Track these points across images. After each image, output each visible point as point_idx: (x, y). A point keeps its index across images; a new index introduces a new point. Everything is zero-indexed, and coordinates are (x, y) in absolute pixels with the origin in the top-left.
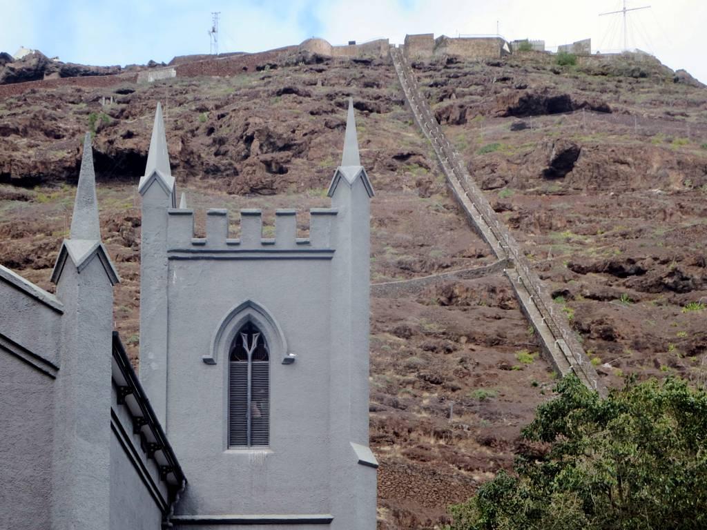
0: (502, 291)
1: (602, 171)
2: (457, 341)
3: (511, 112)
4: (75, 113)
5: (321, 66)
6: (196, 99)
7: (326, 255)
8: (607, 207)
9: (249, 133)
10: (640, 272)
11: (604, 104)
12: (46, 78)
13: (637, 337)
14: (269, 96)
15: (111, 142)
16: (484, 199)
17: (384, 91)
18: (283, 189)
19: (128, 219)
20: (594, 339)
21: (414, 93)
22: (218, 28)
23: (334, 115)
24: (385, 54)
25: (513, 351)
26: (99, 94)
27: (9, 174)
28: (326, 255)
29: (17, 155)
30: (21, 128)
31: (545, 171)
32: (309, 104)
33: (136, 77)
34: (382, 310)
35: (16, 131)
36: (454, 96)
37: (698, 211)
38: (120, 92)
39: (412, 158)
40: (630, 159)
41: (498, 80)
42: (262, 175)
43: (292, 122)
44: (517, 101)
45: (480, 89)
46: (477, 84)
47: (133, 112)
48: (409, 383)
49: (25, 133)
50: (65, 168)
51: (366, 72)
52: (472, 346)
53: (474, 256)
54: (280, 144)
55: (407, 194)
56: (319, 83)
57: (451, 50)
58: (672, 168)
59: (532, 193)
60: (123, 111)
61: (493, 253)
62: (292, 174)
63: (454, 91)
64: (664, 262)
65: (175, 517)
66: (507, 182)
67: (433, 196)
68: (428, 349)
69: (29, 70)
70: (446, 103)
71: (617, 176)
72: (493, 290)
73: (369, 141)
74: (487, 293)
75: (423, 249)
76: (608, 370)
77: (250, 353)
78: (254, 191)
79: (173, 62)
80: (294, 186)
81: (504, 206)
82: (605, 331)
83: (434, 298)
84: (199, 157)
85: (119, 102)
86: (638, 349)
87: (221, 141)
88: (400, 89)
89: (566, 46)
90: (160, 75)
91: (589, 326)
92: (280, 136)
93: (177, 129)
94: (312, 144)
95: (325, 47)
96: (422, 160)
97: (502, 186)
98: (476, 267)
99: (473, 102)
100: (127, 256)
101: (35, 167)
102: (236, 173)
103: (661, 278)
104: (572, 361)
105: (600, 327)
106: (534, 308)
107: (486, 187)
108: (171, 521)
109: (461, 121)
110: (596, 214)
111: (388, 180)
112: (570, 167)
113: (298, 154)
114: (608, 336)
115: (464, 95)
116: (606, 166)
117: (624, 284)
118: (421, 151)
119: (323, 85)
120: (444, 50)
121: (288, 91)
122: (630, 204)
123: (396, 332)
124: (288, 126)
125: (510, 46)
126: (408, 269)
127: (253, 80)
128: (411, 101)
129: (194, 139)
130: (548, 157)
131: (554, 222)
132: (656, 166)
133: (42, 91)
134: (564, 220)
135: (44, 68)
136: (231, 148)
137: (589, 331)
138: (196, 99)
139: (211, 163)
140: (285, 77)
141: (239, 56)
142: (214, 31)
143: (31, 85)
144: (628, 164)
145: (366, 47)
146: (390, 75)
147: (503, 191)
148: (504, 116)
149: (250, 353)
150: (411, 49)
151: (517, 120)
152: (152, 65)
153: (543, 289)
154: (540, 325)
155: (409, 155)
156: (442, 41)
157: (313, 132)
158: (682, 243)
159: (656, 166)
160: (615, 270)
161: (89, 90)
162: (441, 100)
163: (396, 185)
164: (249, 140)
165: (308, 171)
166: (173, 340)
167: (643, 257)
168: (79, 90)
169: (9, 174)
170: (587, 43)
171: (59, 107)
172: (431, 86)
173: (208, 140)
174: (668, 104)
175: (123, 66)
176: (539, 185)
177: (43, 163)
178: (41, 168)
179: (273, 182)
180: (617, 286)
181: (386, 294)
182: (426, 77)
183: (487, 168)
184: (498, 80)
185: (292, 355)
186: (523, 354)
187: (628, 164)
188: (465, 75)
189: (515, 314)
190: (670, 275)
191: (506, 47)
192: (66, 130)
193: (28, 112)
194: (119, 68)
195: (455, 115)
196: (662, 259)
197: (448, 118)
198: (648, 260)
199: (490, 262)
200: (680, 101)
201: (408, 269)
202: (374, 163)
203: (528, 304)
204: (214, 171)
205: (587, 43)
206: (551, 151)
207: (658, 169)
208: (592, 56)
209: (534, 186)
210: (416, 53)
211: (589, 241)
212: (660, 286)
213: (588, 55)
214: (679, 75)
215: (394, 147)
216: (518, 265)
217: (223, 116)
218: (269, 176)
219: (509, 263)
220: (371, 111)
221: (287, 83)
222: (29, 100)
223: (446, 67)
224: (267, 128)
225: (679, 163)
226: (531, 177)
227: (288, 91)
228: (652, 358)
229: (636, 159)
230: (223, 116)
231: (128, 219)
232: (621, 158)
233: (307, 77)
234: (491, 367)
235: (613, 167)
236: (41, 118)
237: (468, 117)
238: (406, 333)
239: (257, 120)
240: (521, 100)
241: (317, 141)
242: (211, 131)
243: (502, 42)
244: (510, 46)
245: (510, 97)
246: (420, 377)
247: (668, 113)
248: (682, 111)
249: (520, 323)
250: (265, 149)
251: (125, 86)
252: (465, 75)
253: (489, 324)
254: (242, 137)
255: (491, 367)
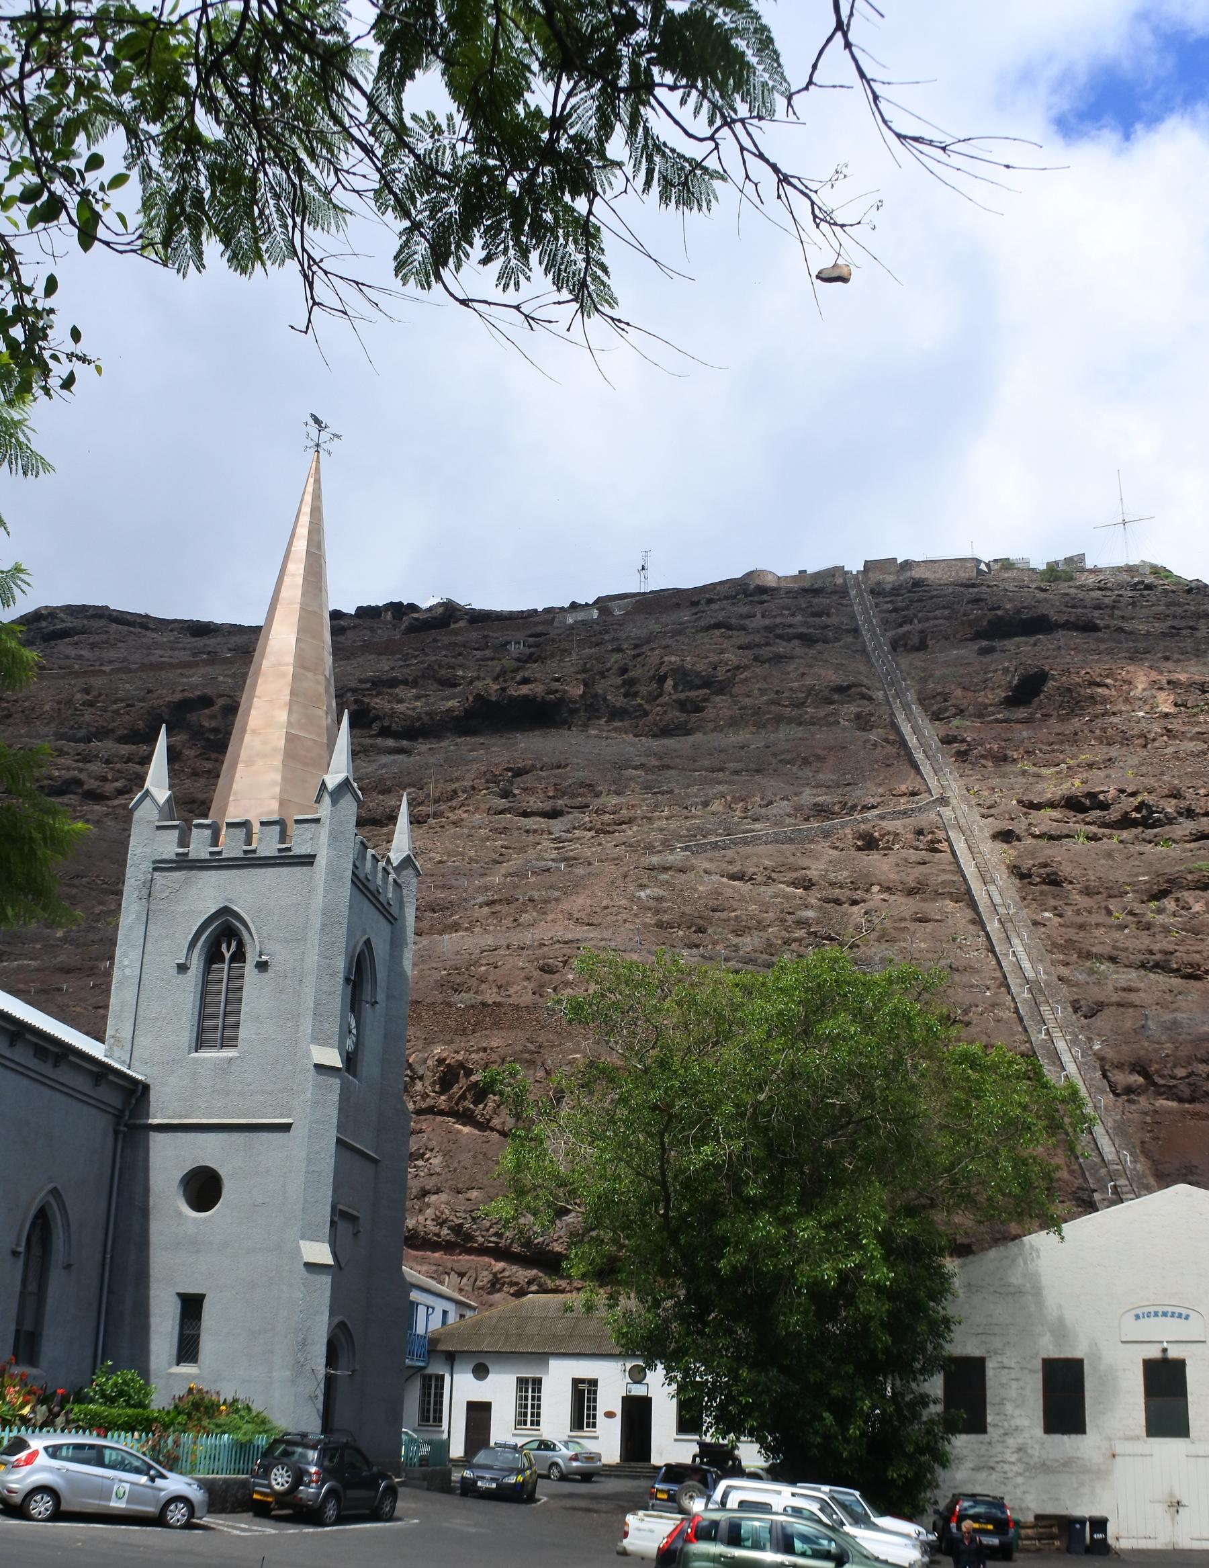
0: (933, 833)
1: (1074, 695)
2: (867, 891)
3: (979, 636)
4: (478, 660)
5: (765, 597)
6: (615, 639)
7: (308, 860)
8: (1076, 734)
9: (662, 671)
10: (1105, 806)
11: (1090, 622)
12: (452, 626)
13: (1088, 880)
14: (697, 631)
15: (504, 689)
16: (931, 731)
17: (834, 620)
18: (698, 729)
19: (508, 769)
20: (1035, 885)
21: (868, 620)
22: (649, 566)
23: (768, 648)
24: (840, 581)
25: (935, 900)
26: (509, 638)
27: (389, 727)
28: (308, 860)
29: (401, 707)
30: (410, 679)
31: (1007, 698)
32: (741, 638)
33: (553, 619)
34: (782, 859)
35: (405, 682)
36: (916, 621)
37: (1189, 735)
38: (530, 636)
39: (853, 690)
40: (1108, 681)
41: (968, 602)
42: (676, 715)
43: (714, 658)
44: (985, 623)
45: (946, 612)
46: (944, 607)
47: (543, 655)
48: (795, 940)
49: (414, 684)
50: (452, 718)
51: (815, 601)
52: (885, 896)
53: (905, 794)
54: (697, 682)
55: (844, 729)
56: (759, 615)
57: (916, 574)
58: (1161, 689)
59: (990, 722)
60: (531, 655)
61: (929, 791)
62: (710, 713)
63: (915, 616)
64: (1133, 794)
65: (132, 1121)
66: (962, 711)
67: (874, 731)
68: (827, 900)
69: (435, 618)
70: (907, 628)
71: (1092, 699)
72: (920, 832)
73: (803, 674)
74: (912, 836)
75: (848, 788)
76: (1049, 919)
77: (227, 956)
78: (665, 732)
79: (596, 602)
80: (711, 725)
81: (955, 737)
82: (1048, 875)
83: (850, 842)
84: (605, 699)
85: (530, 647)
86: (1088, 895)
87: (631, 682)
88: (853, 617)
89: (1057, 563)
90: (581, 616)
91: (1030, 869)
92: (698, 674)
93: (584, 671)
94: (737, 680)
95: (770, 577)
96: (865, 690)
97: (954, 716)
98: (758, 826)
99: (935, 626)
100: (501, 807)
101: (419, 718)
102: (646, 714)
103: (1127, 813)
104: (1002, 910)
105: (1042, 871)
106: (966, 851)
107: (936, 717)
108: (125, 1125)
109: (922, 647)
110: (1061, 742)
111: (822, 714)
112: (1037, 692)
113: (721, 691)
114: (1054, 881)
115: (928, 619)
116: (1079, 689)
117: (1083, 820)
118: (866, 681)
119: (763, 616)
120: (909, 574)
121: (718, 626)
122: (1104, 730)
123: (794, 884)
124: (710, 663)
125: (988, 565)
126: (825, 811)
127: (685, 616)
128: (864, 629)
129: (603, 681)
130: (1010, 682)
131: (1009, 753)
132: (1140, 687)
133: (446, 640)
134: (1021, 751)
135: (450, 616)
136: (642, 688)
137: (1029, 876)
138: (615, 639)
139: (618, 704)
140: (718, 612)
141: (633, 600)
142: (643, 569)
143: (434, 633)
144: (1107, 686)
145: (818, 575)
146: (845, 602)
147: (956, 722)
148: (971, 640)
149: (227, 956)
150: (871, 574)
151: (984, 643)
152: (574, 606)
153: (981, 829)
154: (970, 869)
155: (849, 687)
156: (907, 564)
157: (738, 668)
158: (1158, 771)
159: (1140, 687)
160: (1073, 804)
161: (497, 636)
162: (901, 626)
163: (832, 720)
164: (662, 680)
165: (728, 708)
166: (149, 947)
167: (1105, 789)
168: (486, 637)
169: (389, 727)
170: (1082, 557)
171: (460, 654)
172: (890, 612)
173: (619, 681)
174: (1175, 617)
175: (540, 610)
176: (999, 713)
177: (427, 714)
178: (426, 718)
179: (686, 722)
180: (1075, 824)
181: (791, 839)
182: (887, 602)
183: (938, 697)
184: (968, 602)
185: (264, 958)
186: (950, 905)
187: (1107, 686)
188: (932, 598)
189: (947, 856)
190: (1138, 809)
191: (983, 567)
192: (463, 678)
193: (422, 662)
194: (535, 611)
195: (915, 640)
196: (1129, 791)
197: (905, 645)
198: (1112, 793)
199: (924, 799)
200: (1188, 614)
201: (825, 811)
202: (807, 697)
203: (960, 846)
204: (616, 714)
205: (1082, 557)
206: (1013, 676)
207: (1144, 690)
208: (1088, 571)
209: (994, 714)
210: (875, 577)
211: (1045, 772)
212: (1125, 822)
213: (1083, 570)
214: (1193, 585)
215: (833, 678)
216: (954, 802)
217: (639, 655)
218: (683, 717)
219: (943, 801)
220: (816, 641)
221: (721, 616)
222: (427, 650)
223: (909, 592)
224: (682, 666)
225: (1169, 682)
226: (991, 705)
227: (718, 626)
228: (1103, 904)
229: (1116, 680)
230: (639, 655)
231: (508, 769)
232: (1098, 680)
233: (744, 610)
234: (903, 919)
235: (1088, 691)
236: (436, 667)
237: (930, 643)
238: (808, 885)
239: (673, 659)
240: (989, 621)
241: (743, 676)
242: (624, 670)
243: (979, 561)
244: (988, 565)
245: (977, 619)
246: (810, 934)
247: (1173, 627)
248: (1191, 624)
249: (948, 868)
250: (680, 688)
251: (540, 629)
252: (932, 598)
253: (909, 870)
254: (654, 676)
255: (903, 919)
